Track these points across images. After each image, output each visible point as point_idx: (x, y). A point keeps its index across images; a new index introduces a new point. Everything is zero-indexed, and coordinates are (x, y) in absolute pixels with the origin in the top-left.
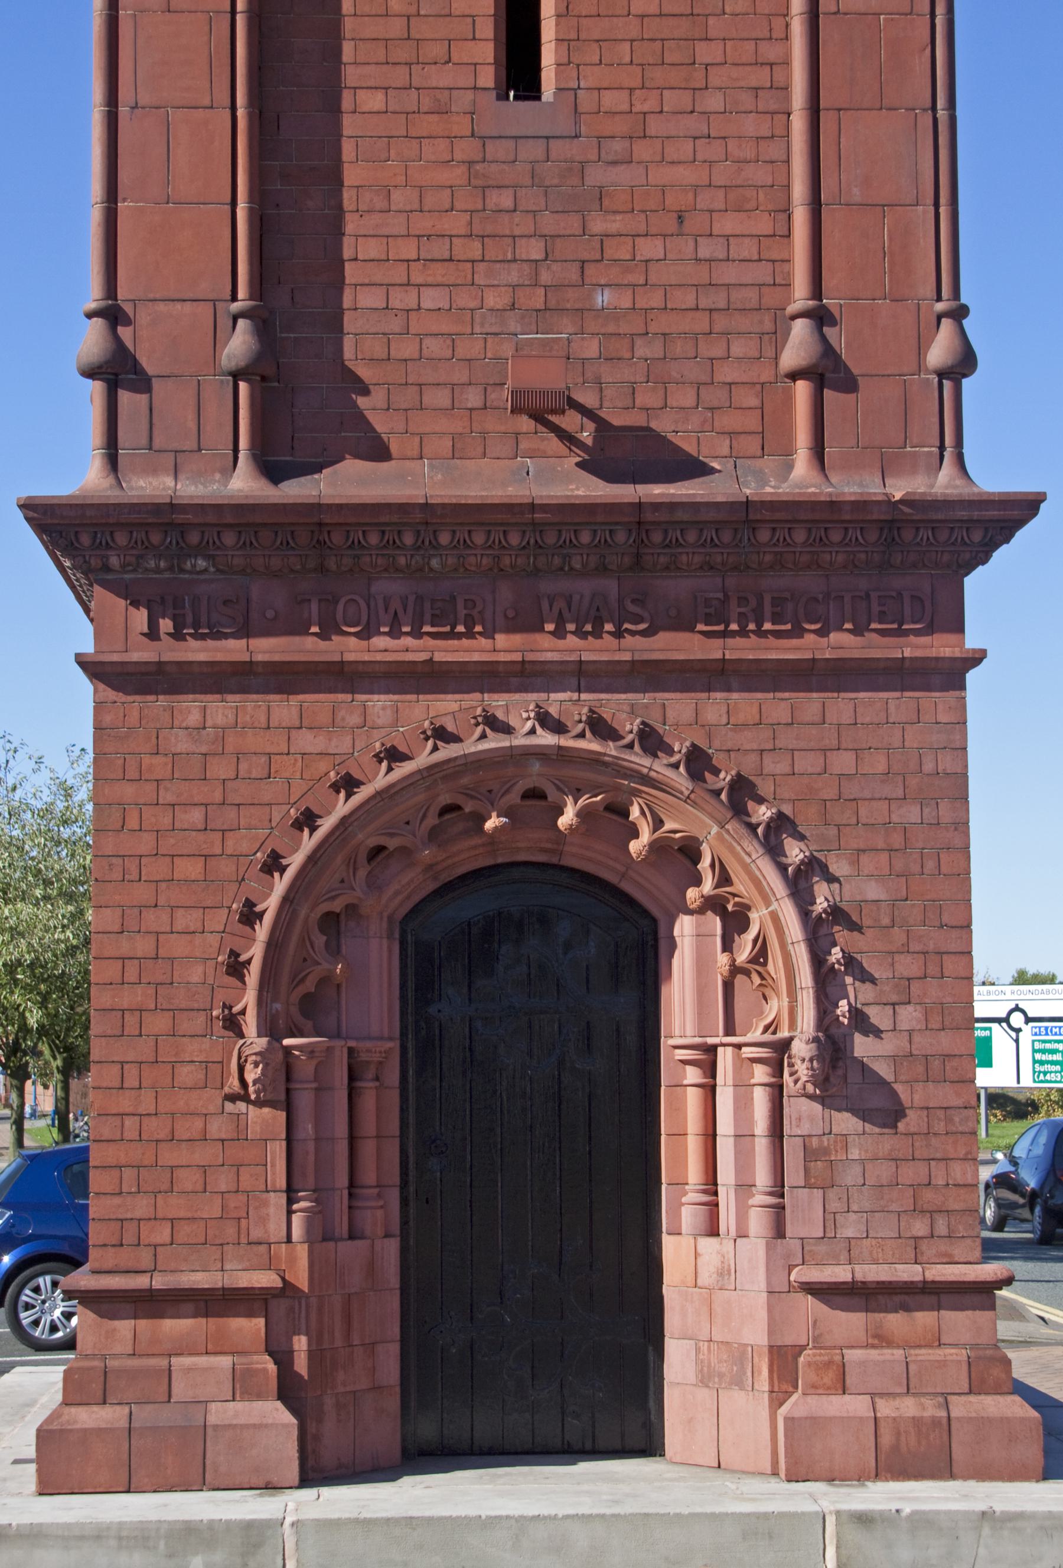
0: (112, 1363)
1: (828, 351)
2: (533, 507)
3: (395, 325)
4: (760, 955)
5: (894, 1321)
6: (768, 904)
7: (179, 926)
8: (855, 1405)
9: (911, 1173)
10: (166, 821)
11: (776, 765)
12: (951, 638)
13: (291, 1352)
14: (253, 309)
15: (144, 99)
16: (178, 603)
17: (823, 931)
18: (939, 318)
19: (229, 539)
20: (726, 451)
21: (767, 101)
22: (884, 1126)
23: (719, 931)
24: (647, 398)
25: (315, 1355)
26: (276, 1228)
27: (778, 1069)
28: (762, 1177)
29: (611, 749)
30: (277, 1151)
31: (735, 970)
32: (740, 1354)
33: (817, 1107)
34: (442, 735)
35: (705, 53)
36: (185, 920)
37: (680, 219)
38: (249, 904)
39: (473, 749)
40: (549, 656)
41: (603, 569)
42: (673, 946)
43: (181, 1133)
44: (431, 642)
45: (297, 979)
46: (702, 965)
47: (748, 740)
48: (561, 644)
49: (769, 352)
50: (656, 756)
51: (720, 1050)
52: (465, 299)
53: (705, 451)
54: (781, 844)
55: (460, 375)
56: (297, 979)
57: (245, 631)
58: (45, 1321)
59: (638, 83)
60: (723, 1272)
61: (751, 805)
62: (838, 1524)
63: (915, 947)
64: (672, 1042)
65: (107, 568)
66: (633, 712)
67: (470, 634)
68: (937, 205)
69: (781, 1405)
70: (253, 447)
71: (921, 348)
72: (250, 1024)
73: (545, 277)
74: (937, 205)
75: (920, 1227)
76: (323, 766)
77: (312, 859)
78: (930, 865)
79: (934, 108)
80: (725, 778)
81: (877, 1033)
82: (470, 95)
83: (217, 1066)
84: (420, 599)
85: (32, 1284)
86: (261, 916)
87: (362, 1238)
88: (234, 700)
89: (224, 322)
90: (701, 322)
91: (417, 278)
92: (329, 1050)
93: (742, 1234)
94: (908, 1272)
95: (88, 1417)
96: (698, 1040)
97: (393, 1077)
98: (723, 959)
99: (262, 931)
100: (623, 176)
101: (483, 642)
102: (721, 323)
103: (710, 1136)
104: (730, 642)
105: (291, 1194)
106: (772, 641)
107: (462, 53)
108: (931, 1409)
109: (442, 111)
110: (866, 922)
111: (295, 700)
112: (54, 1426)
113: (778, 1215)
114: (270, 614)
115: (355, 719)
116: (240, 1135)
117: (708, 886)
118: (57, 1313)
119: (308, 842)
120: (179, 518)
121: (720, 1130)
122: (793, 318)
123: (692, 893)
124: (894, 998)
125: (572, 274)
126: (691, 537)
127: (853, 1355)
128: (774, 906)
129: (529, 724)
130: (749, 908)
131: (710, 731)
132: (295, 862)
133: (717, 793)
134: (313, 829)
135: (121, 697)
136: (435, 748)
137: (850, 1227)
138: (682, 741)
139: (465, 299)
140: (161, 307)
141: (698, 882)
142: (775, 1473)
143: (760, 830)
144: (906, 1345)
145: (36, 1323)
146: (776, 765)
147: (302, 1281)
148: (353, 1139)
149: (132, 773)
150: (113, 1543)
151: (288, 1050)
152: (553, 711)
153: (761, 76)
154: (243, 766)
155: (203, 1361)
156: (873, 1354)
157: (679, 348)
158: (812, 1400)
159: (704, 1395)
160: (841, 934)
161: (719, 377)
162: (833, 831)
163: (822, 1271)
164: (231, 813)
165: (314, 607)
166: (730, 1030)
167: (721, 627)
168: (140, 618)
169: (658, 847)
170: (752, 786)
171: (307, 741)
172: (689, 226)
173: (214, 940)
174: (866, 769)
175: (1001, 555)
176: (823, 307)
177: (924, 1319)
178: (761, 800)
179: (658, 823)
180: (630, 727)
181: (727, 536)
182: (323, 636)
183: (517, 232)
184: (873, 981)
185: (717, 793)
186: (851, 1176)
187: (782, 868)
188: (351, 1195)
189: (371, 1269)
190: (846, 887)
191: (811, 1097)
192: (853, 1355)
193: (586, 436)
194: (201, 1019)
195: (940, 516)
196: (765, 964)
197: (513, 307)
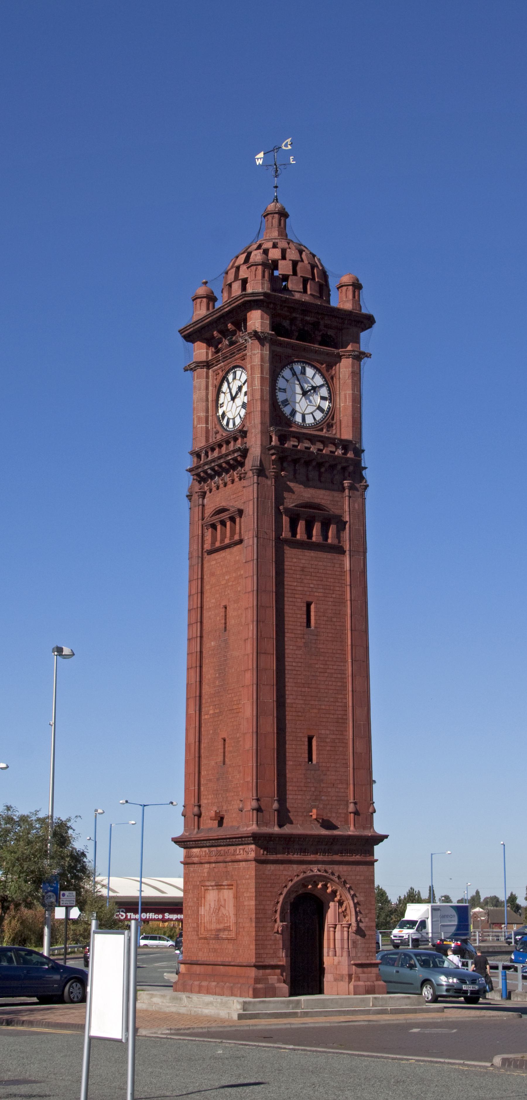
3: (294, 801)
5: (365, 970)
16: (267, 849)
24: (329, 815)
33: (354, 935)
36: (268, 903)
42: (329, 907)
47: (345, 874)
60: (339, 962)
73: (315, 794)
75: (368, 955)
76: (287, 877)
80: (343, 880)
88: (275, 865)
91: (297, 793)
94: (368, 962)
95: (259, 986)
101: (309, 856)
105: (283, 949)
106: (348, 857)
108: (372, 984)
109: (300, 765)
110: (361, 904)
115: (291, 869)
127: (360, 975)
153: (344, 762)
155: (272, 977)
156: (363, 975)
160: (358, 906)
163: (174, 999)
166: (339, 922)
169: (332, 891)
171: (285, 873)
175: (381, 844)
177: (369, 969)
180: (330, 871)
186: (359, 946)
191: (354, 933)
192: (360, 975)
193: (321, 821)
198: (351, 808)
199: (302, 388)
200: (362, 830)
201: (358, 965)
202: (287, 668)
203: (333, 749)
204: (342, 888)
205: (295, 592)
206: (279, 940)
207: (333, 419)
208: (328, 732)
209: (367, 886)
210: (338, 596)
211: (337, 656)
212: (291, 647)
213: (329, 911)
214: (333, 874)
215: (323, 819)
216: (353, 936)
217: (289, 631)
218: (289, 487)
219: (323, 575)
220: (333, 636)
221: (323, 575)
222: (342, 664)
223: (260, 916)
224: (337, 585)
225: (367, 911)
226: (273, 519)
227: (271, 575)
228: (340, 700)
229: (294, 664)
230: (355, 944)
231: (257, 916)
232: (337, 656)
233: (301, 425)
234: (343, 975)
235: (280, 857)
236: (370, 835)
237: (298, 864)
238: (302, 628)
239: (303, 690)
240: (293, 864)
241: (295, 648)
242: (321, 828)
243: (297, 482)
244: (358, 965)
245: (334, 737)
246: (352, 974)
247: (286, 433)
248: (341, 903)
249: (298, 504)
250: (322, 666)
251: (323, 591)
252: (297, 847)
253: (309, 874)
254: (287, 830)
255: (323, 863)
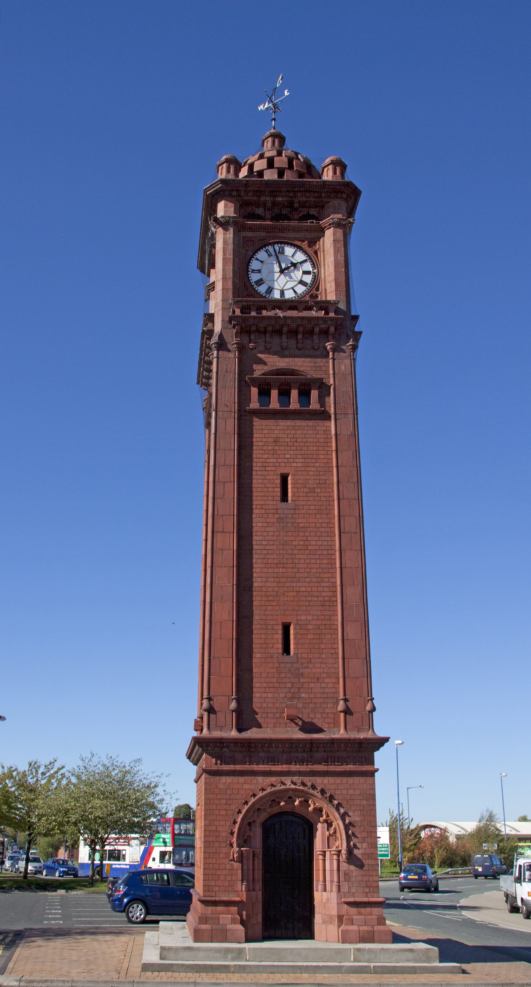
0: (208, 916)
1: (347, 707)
2: (291, 739)
3: (262, 700)
4: (335, 832)
5: (363, 910)
6: (336, 821)
7: (221, 824)
8: (355, 928)
9: (365, 878)
10: (218, 802)
11: (338, 792)
12: (372, 766)
13: (242, 915)
14: (236, 698)
15: (216, 656)
16: (221, 757)
17: (347, 827)
18: (368, 700)
19: (232, 745)
20: (327, 726)
21: (334, 656)
22: (360, 868)
23: (326, 827)
24: (312, 716)
25: (247, 915)
26: (239, 889)
27: (339, 857)
28: (336, 879)
29: (305, 789)
30: (240, 872)
31: (330, 835)
32: (331, 917)
34: (272, 785)
35: (322, 646)
36: (221, 823)
37: (318, 679)
38: (235, 820)
39: (279, 788)
40: (294, 769)
41: (304, 751)
42: (317, 830)
43: (221, 868)
44: (270, 766)
45: (244, 836)
46: (323, 834)
48: (295, 767)
49: (335, 706)
50: (314, 790)
51: (327, 852)
52: (276, 695)
53: (323, 726)
54: (339, 809)
55: (275, 711)
56: (244, 836)
57: (234, 764)
58: (135, 916)
59: (309, 652)
60: (328, 899)
61: (333, 800)
62: (354, 951)
63: (366, 830)
64: (316, 850)
65: (208, 750)
66: (310, 781)
67: (278, 765)
68: (367, 677)
69: (340, 927)
70: (236, 725)
71: (365, 706)
72: (235, 845)
73: (292, 691)
74: (367, 677)
75: (367, 890)
76: (249, 791)
77: (247, 811)
78: (369, 813)
79: (366, 658)
80: (328, 795)
81: (358, 849)
82: (277, 654)
83: (228, 854)
84: (268, 757)
85: (132, 906)
86: (237, 822)
87: (255, 891)
88: (232, 777)
89: (230, 700)
90: (322, 700)
91: (267, 691)
92: (249, 851)
93: (331, 891)
94: (365, 899)
95: (204, 927)
96: (322, 850)
97: (261, 857)
98: (327, 833)
99: (237, 826)
100: (306, 671)
101: (281, 766)
102: (326, 700)
103: (324, 870)
104: (329, 767)
105: (242, 881)
106: (337, 767)
107: (276, 646)
108: (370, 929)
109: (272, 657)
110: (356, 825)
111: (243, 778)
112: (197, 928)
113: (339, 887)
114: (239, 760)
115: (255, 782)
116: (232, 869)
117: (324, 817)
118: (138, 914)
119: (246, 807)
120: (223, 741)
121: (326, 869)
122: (340, 700)
123: (321, 819)
124: (362, 841)
125: (297, 690)
126: (322, 745)
127: (354, 917)
128: (338, 822)
129: (289, 783)
130: (332, 822)
131: (325, 785)
132: (244, 811)
133: (326, 798)
134: (247, 804)
135: (210, 777)
136: (271, 788)
137: (353, 890)
138: (320, 787)
139: (276, 695)
140: (219, 697)
141: (322, 816)
142: (339, 942)
143: (335, 806)
144: (365, 915)
145: (133, 917)
146: (338, 792)
147: (245, 899)
148: (253, 870)
149: (212, 792)
150: (214, 951)
151: (242, 851)
152: (294, 781)
153: (333, 651)
154: (233, 791)
155: (225, 916)
156: (358, 917)
157: (318, 705)
158: (346, 926)
159: (324, 926)
160: (351, 828)
161: (325, 712)
162: (349, 806)
164: (231, 801)
165: (248, 758)
166: (328, 848)
167: (327, 764)
168: (214, 760)
169: (315, 809)
170: (333, 797)
171: (246, 786)
172: (320, 681)
173: (227, 827)
174: (356, 793)
175: (382, 749)
176: (346, 698)
177: (368, 910)
178: (335, 800)
179: (315, 804)
180: (309, 784)
181: (328, 745)
182: (249, 765)
183: (286, 682)
184: (357, 838)
185: (326, 798)
186: (353, 879)
187: (339, 814)
188: (253, 882)
189: (257, 898)
190: (352, 818)
191: (346, 862)
193: (300, 723)
194: (225, 844)
195: (370, 742)
196: (336, 834)
197: (285, 697)
198: (341, 706)
199: (280, 266)
200: (356, 733)
201: (349, 904)
202: (255, 547)
203: (317, 637)
204: (327, 805)
205: (266, 464)
206: (237, 870)
207: (317, 289)
208: (310, 617)
209: (364, 802)
210: (322, 465)
211: (322, 530)
212: (260, 524)
213: (317, 833)
214: (313, 787)
215: (303, 722)
216: (344, 866)
217: (258, 507)
218: (260, 358)
219: (302, 444)
220: (317, 508)
221: (302, 444)
222: (329, 539)
223: (211, 839)
224: (322, 452)
225: (364, 834)
226: (236, 391)
227: (233, 448)
228: (327, 580)
229: (264, 543)
230: (347, 877)
231: (207, 840)
232: (322, 530)
233: (262, 295)
234: (332, 915)
235: (238, 767)
236: (362, 738)
237: (264, 776)
238: (275, 503)
239: (276, 570)
240: (258, 776)
241: (265, 525)
242: (300, 731)
243: (269, 353)
244: (349, 904)
245: (319, 622)
246: (343, 916)
247: (249, 304)
248: (330, 825)
249: (265, 373)
250: (302, 543)
251: (303, 460)
252: (262, 754)
253: (279, 787)
254: (252, 734)
255: (300, 773)
